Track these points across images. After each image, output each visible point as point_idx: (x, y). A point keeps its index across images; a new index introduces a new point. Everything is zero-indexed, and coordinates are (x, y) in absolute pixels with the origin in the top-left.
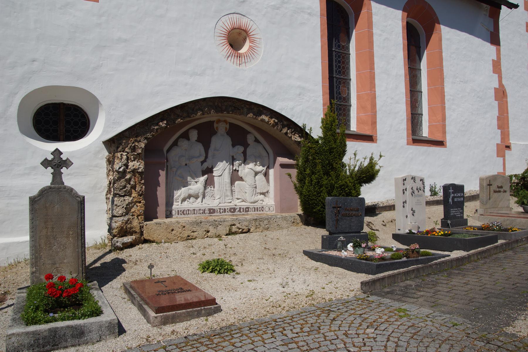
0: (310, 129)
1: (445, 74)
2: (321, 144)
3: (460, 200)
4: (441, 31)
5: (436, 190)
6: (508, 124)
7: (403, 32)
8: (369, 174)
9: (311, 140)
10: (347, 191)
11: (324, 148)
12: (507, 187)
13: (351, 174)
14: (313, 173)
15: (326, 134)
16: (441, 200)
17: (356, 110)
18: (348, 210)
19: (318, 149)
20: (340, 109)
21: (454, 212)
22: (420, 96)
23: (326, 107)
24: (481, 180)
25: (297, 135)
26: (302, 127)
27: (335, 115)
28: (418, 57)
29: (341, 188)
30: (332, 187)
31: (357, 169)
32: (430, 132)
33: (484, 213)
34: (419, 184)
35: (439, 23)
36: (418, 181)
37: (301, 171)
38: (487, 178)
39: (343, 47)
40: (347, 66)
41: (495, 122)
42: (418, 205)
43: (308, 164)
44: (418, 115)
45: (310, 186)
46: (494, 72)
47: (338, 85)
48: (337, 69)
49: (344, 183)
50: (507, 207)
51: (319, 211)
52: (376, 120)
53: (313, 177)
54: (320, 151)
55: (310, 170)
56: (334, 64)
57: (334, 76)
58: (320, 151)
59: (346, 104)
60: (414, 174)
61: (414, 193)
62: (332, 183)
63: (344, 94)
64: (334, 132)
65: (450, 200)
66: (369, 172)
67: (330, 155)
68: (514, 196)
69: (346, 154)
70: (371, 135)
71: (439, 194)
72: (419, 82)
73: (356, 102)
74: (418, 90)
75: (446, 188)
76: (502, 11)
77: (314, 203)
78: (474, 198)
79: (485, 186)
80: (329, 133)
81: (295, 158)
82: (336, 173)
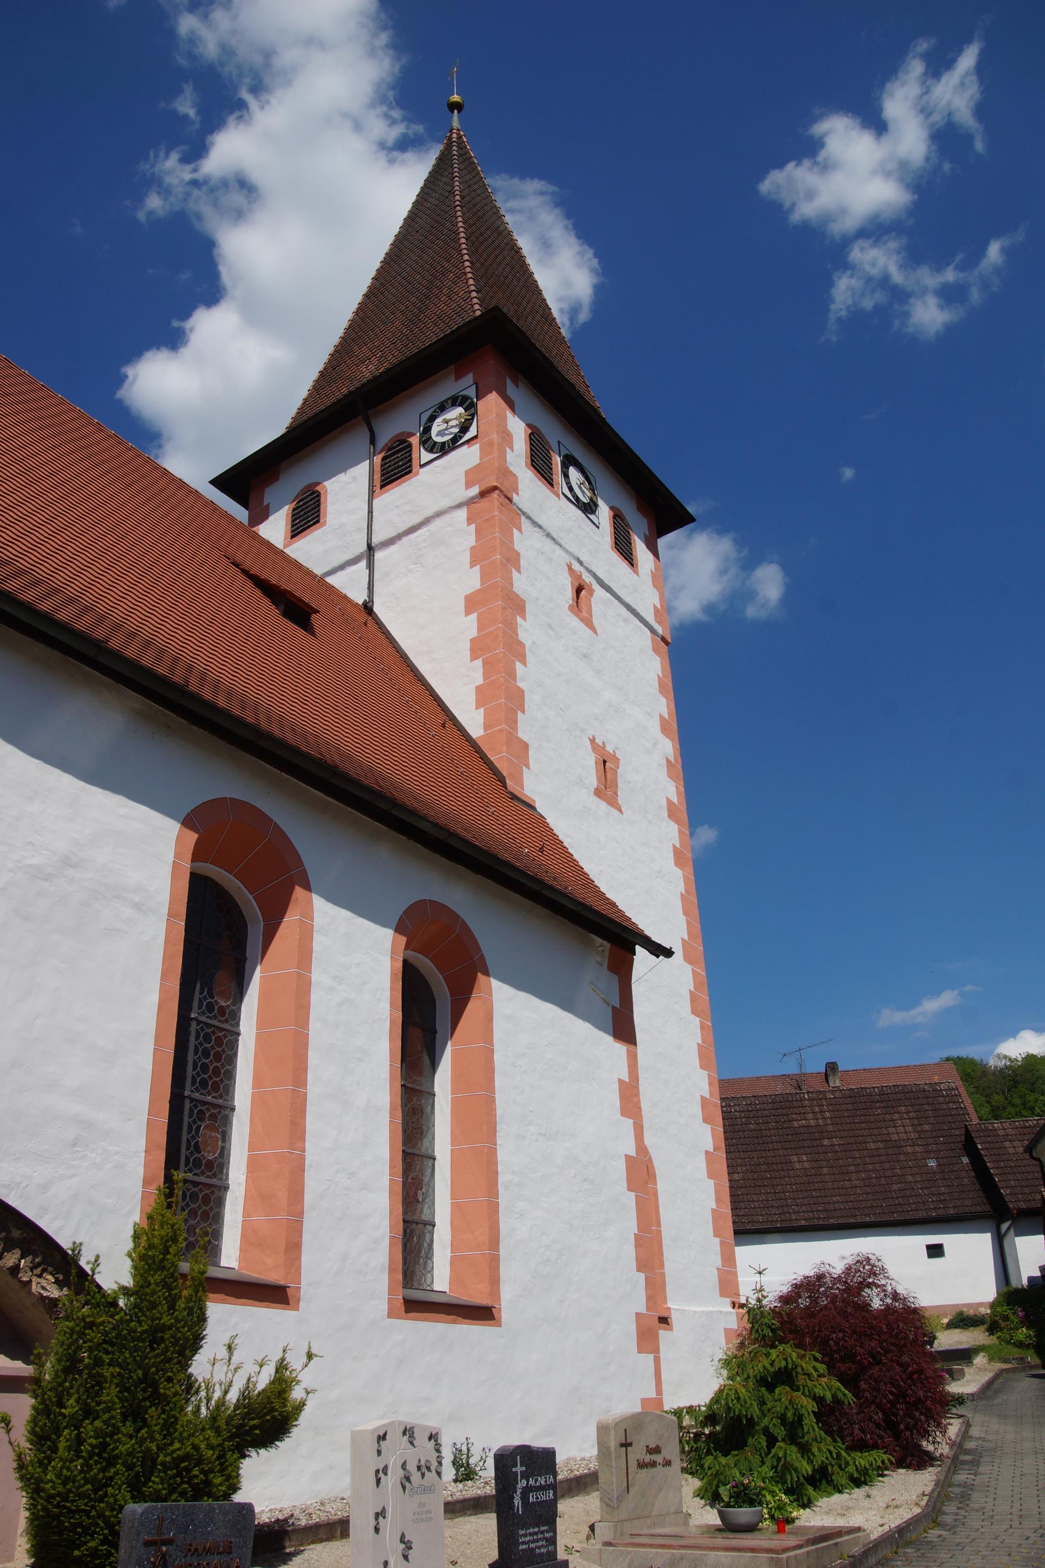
0: (93, 1260)
1: (499, 1112)
2: (126, 1314)
3: (544, 1498)
4: (491, 995)
5: (472, 1461)
6: (662, 1255)
7: (392, 988)
8: (273, 1417)
9: (93, 1297)
10: (196, 1476)
11: (133, 1324)
12: (672, 1451)
13: (213, 1418)
14: (88, 1413)
15: (146, 1280)
16: (486, 1497)
17: (241, 1201)
18: (196, 1550)
19: (114, 1328)
20: (194, 1197)
21: (528, 1538)
22: (429, 1170)
23: (153, 1190)
24: (603, 1429)
25: (49, 1277)
26: (70, 1252)
27: (179, 1219)
28: (429, 1055)
29: (177, 1467)
30: (149, 1463)
31: (233, 1396)
32: (455, 1278)
33: (614, 1539)
34: (425, 1450)
35: (487, 973)
36: (421, 1438)
37: (46, 1406)
38: (617, 1424)
39: (222, 1011)
40: (227, 1067)
41: (630, 1251)
42: (422, 1520)
43: (75, 1379)
44: (420, 1226)
45: (71, 1461)
46: (624, 1113)
47: (194, 1122)
48: (198, 1074)
49: (188, 1449)
50: (675, 1513)
51: (94, 1553)
52: (301, 1236)
53: (89, 1428)
54: (119, 1336)
55: (78, 1401)
56: (191, 1057)
57: (187, 1093)
58: (119, 1336)
59: (213, 1181)
60: (410, 1420)
61: (410, 1482)
62: (149, 1450)
63: (209, 1152)
64: (172, 1275)
65: (517, 1501)
66: (273, 1410)
67: (153, 1349)
68: (690, 1474)
69: (201, 1347)
70: (282, 1283)
71: (480, 1473)
72: (429, 1128)
73: (243, 1178)
74: (423, 1150)
75: (505, 1460)
76: (637, 958)
77: (80, 1525)
78: (582, 1484)
79: (613, 1449)
80: (156, 1277)
81: (32, 1357)
82: (164, 1412)
